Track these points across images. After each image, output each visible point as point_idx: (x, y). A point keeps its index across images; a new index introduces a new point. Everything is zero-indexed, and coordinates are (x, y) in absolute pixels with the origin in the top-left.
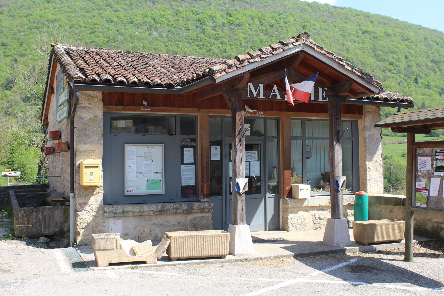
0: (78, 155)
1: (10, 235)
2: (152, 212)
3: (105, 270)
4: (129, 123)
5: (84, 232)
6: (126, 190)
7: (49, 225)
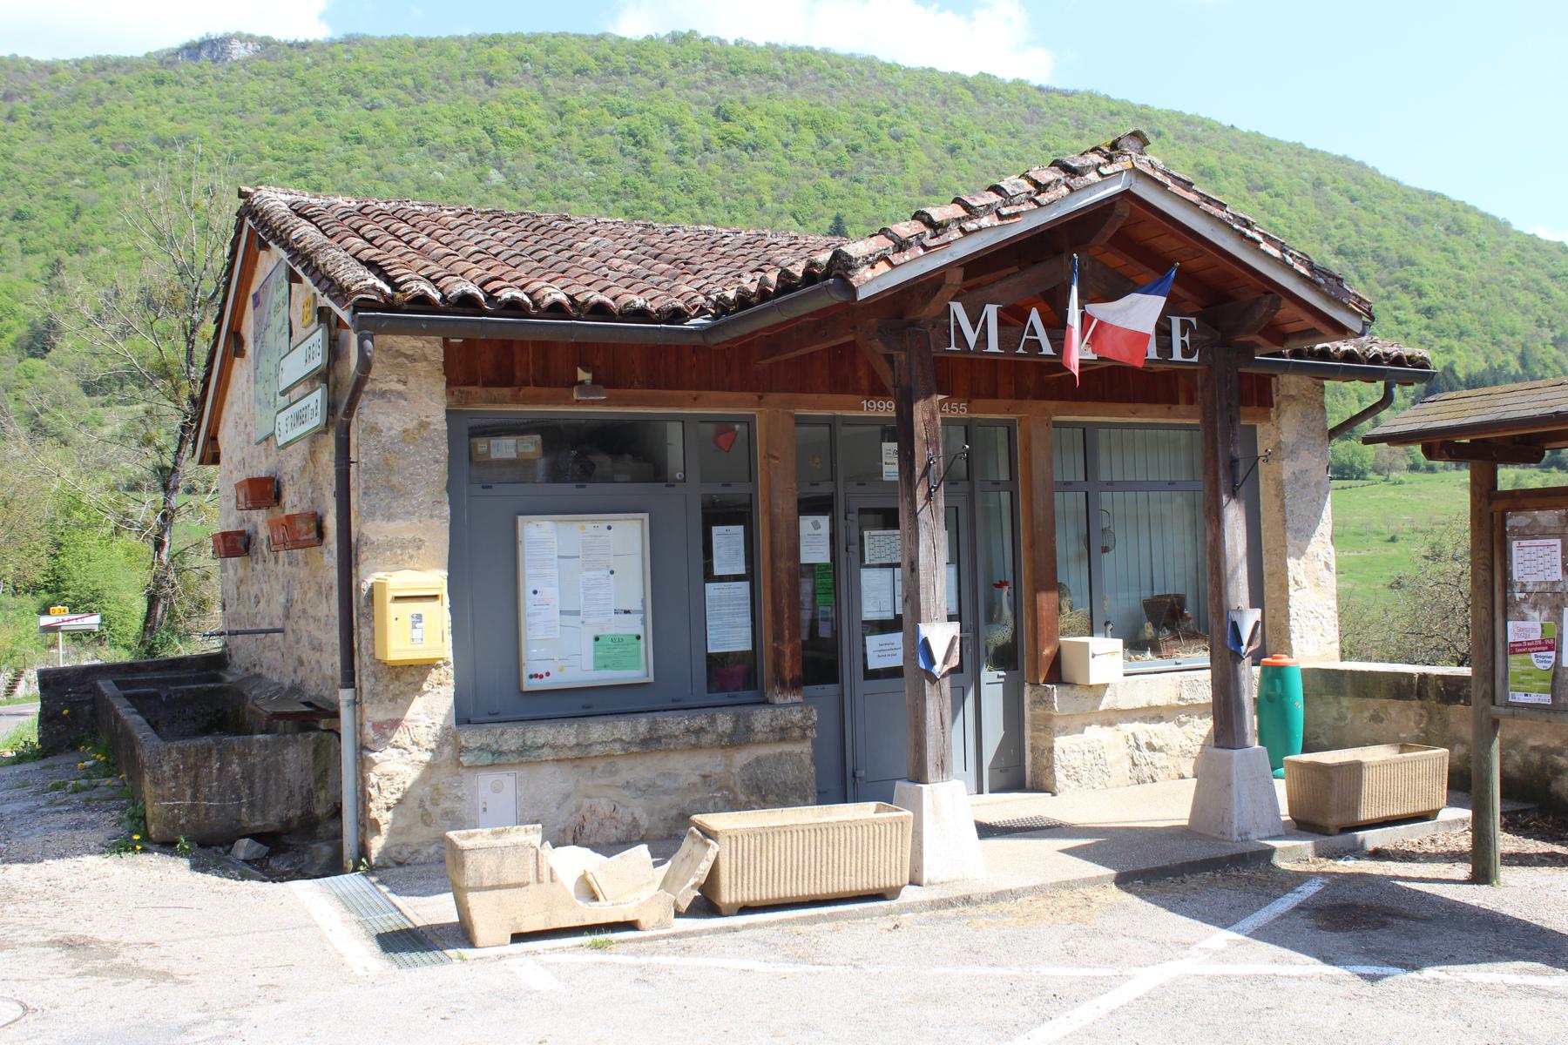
0: (365, 555)
1: (136, 837)
2: (618, 746)
3: (501, 957)
4: (530, 446)
5: (394, 819)
6: (526, 671)
7: (265, 795)
